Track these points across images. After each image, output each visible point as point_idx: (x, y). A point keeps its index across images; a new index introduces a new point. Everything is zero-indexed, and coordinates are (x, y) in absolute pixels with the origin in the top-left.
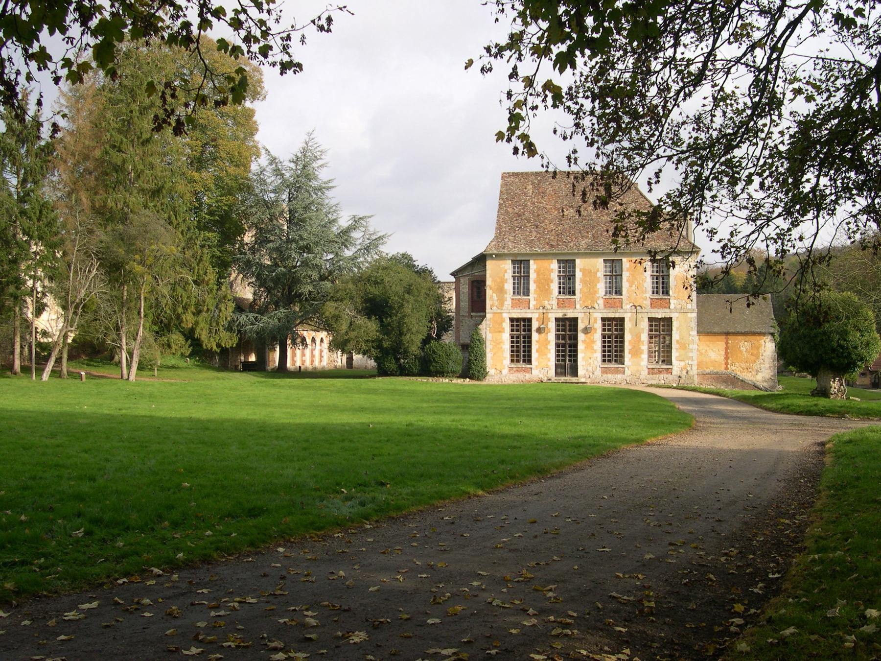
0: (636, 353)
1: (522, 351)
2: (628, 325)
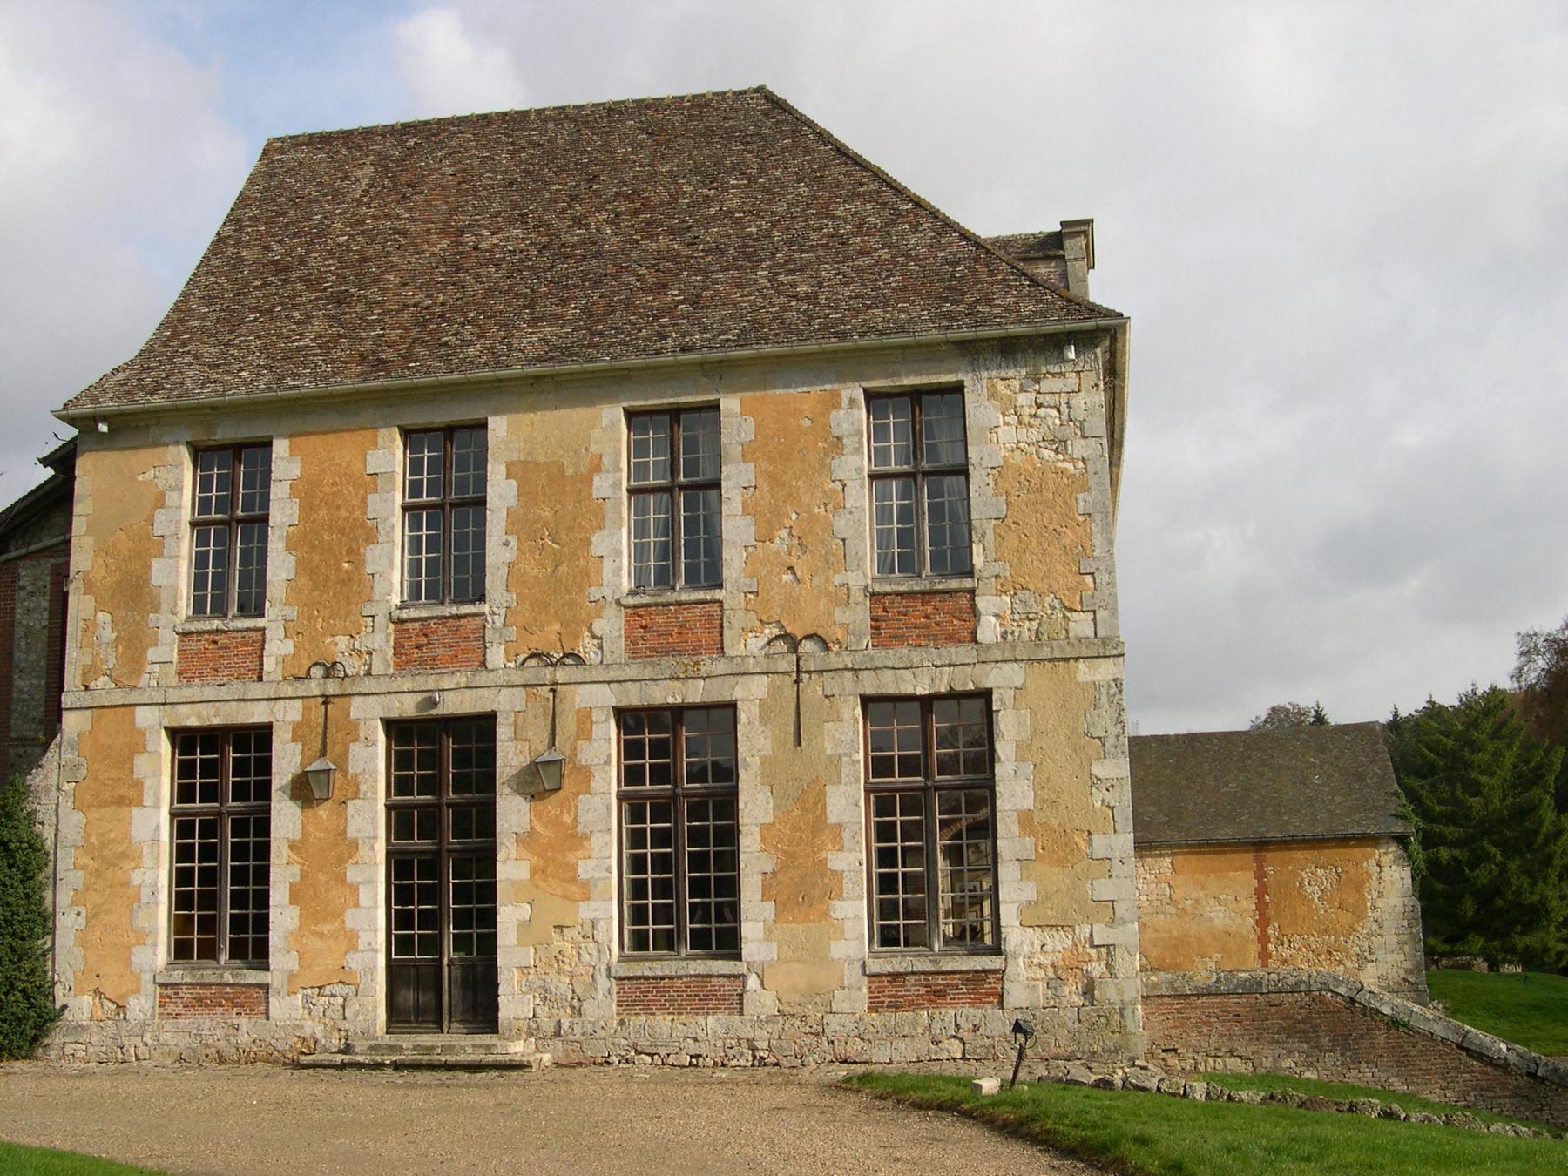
0: (803, 891)
2: (755, 744)
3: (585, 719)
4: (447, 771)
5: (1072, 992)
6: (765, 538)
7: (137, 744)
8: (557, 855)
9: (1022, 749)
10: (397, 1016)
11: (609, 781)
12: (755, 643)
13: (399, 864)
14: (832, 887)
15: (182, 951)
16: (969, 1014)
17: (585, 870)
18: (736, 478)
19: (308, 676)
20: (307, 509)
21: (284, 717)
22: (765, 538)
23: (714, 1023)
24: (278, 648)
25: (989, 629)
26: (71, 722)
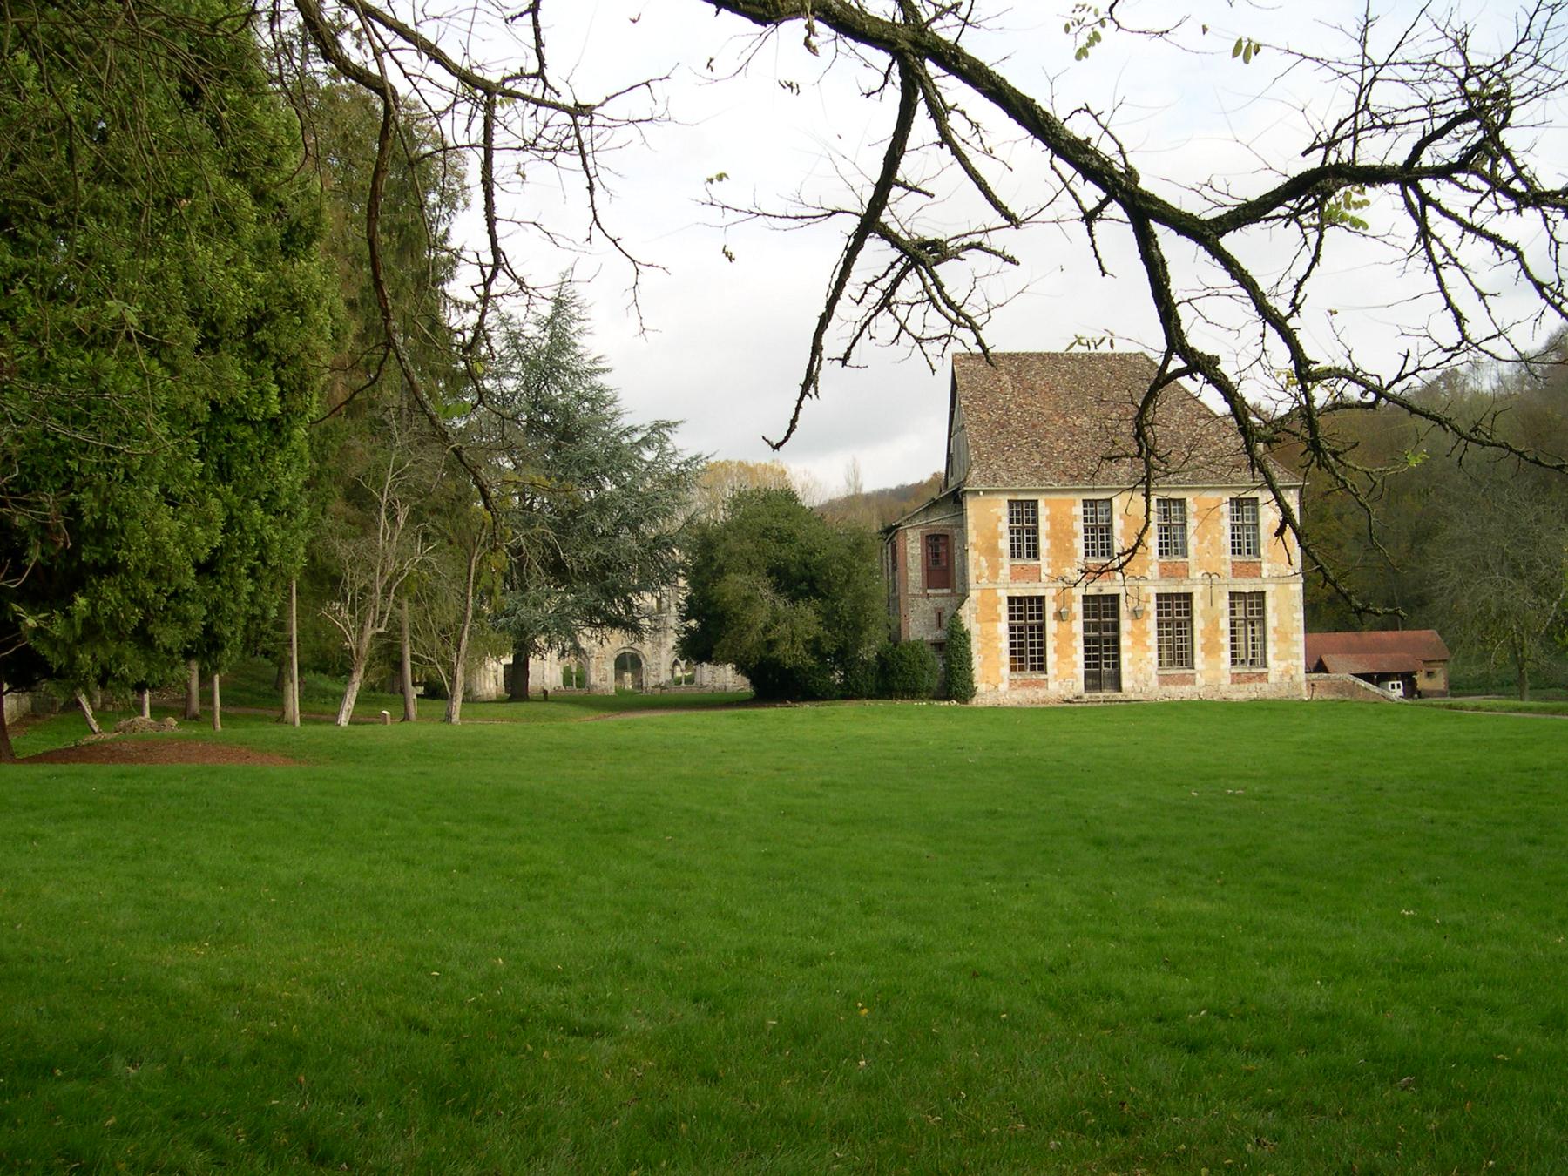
0: (1212, 649)
1: (1028, 651)
2: (1198, 605)
3: (1148, 596)
4: (1103, 616)
5: (1287, 679)
6: (1201, 543)
7: (998, 602)
8: (1139, 639)
9: (1274, 609)
10: (1087, 687)
11: (1154, 616)
12: (1199, 575)
13: (1086, 641)
14: (1221, 648)
15: (1013, 669)
16: (1259, 685)
17: (1148, 643)
18: (1192, 524)
19: (253, 603)
20: (1053, 525)
21: (1049, 593)
22: (1201, 543)
23: (1187, 688)
24: (1045, 570)
25: (1265, 574)
26: (973, 594)
